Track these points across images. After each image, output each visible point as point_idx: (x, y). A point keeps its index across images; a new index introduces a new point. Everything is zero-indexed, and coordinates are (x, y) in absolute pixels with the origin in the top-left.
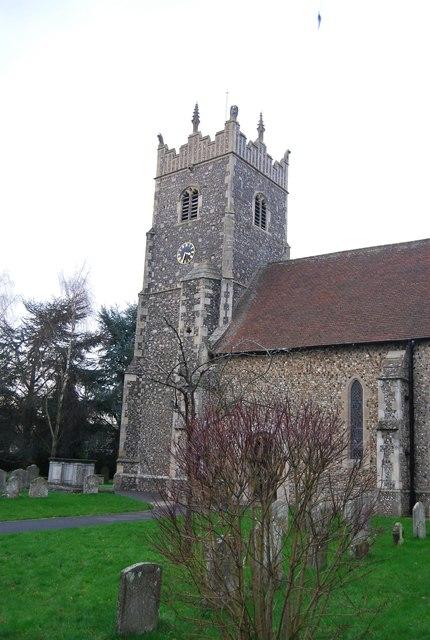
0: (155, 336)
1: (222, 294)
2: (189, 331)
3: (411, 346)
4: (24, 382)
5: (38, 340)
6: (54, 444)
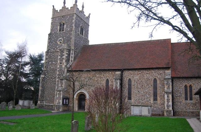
1: (71, 54)
2: (61, 63)
3: (122, 71)
4: (5, 76)
5: (9, 63)
6: (15, 95)
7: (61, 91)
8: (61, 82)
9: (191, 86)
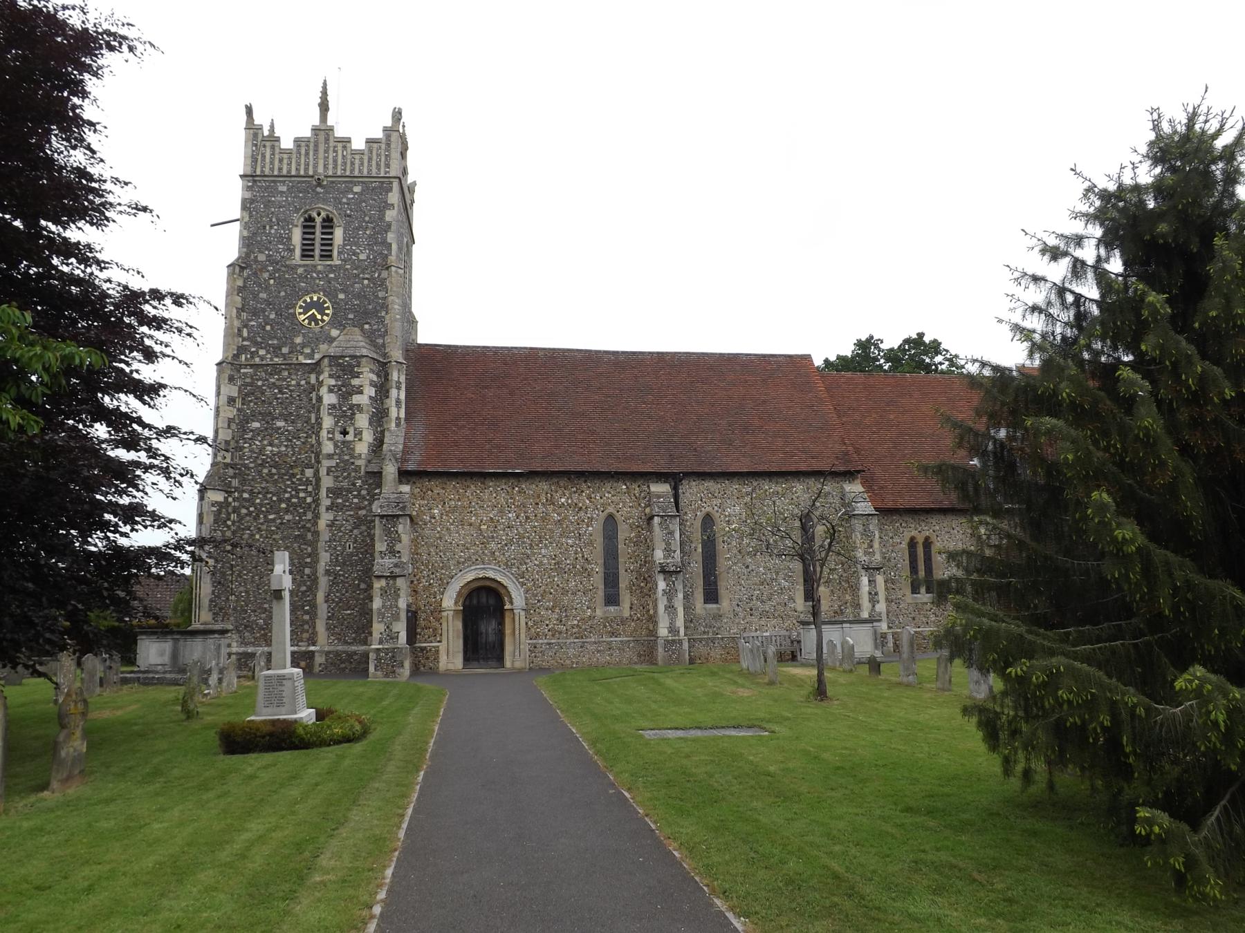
0: (257, 432)
7: (394, 577)
8: (388, 532)
9: (927, 543)
